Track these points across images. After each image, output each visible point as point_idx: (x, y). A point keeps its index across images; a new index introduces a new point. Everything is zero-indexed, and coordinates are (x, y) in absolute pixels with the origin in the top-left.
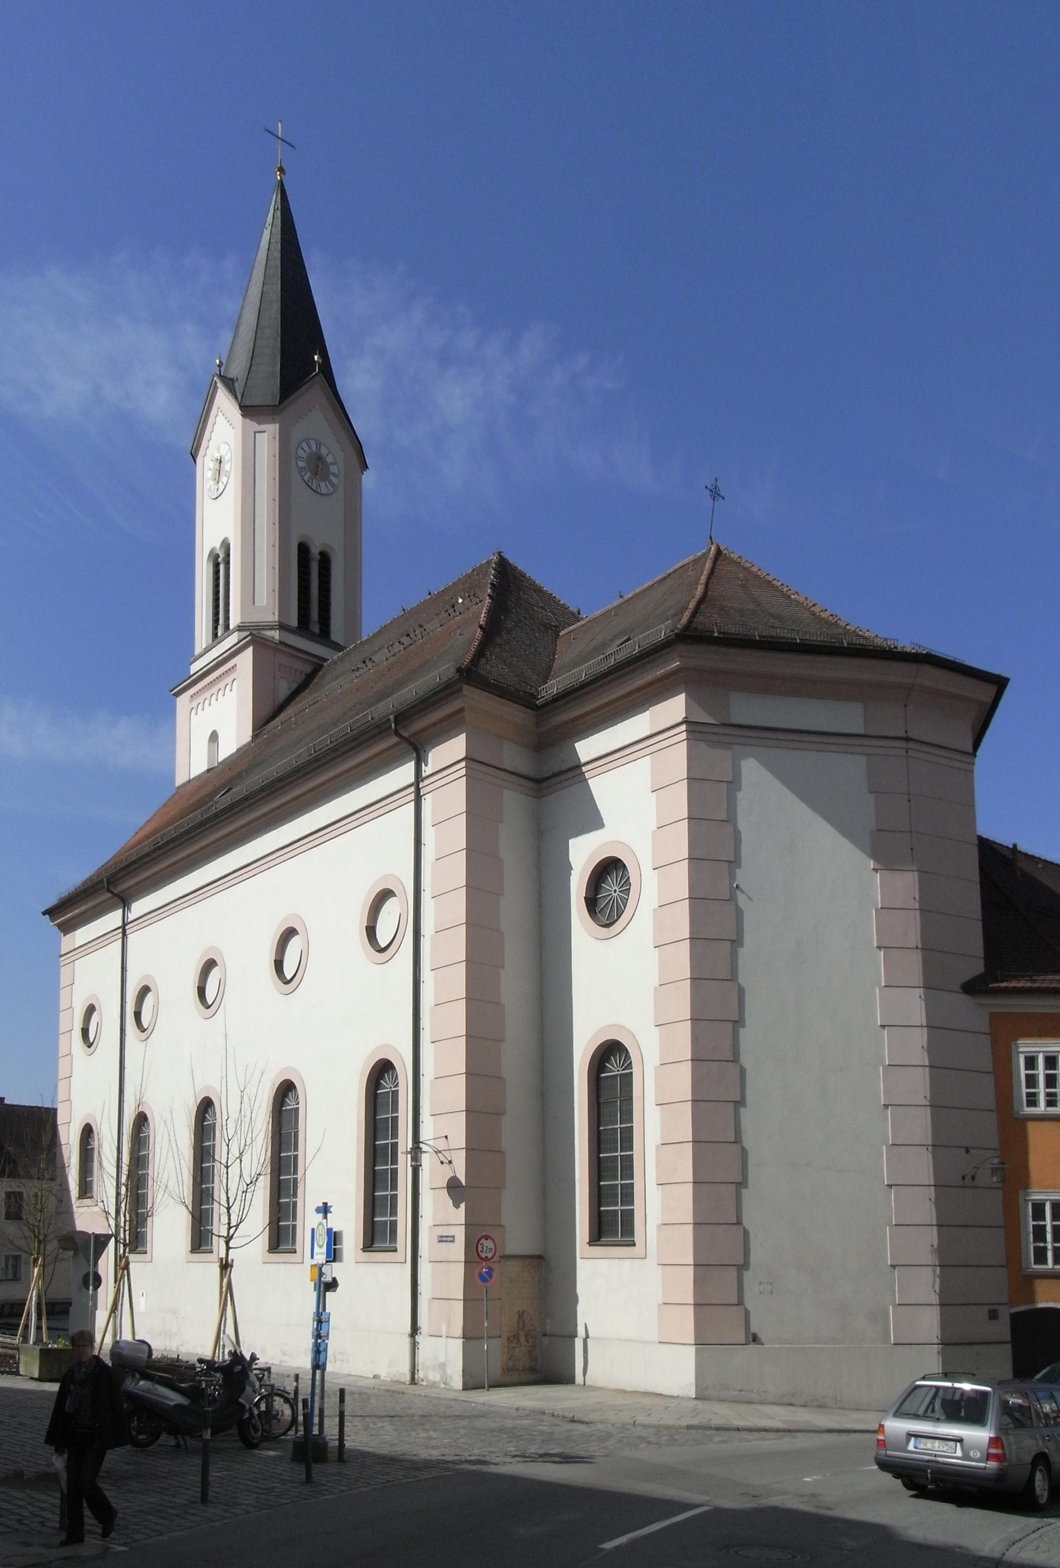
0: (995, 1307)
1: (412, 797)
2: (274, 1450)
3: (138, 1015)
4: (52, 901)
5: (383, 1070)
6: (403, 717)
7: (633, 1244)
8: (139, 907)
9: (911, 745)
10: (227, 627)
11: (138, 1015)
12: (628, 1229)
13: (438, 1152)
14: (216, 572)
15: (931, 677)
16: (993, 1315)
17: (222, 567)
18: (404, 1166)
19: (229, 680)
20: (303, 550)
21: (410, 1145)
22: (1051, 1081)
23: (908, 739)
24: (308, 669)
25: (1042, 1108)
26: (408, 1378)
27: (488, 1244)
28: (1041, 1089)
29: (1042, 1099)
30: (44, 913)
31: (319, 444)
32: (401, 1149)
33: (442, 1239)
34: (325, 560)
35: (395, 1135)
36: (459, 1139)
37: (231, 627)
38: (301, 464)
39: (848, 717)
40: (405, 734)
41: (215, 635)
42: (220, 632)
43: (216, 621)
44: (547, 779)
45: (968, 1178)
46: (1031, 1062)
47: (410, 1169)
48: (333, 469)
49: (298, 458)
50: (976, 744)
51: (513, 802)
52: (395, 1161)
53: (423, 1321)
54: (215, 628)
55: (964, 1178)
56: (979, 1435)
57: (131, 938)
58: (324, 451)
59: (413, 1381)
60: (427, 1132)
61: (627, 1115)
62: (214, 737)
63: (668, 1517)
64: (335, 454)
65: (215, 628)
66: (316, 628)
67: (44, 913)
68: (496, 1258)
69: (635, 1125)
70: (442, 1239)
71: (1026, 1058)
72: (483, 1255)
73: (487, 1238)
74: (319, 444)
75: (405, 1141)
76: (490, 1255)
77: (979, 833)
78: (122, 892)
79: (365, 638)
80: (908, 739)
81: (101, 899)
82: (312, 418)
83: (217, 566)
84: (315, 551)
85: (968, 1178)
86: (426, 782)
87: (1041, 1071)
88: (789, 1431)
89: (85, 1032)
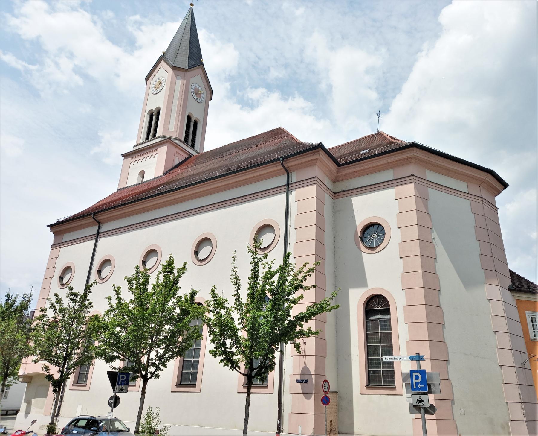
1: (285, 190)
3: (99, 272)
4: (54, 222)
10: (155, 135)
17: (154, 117)
20: (189, 118)
24: (187, 156)
30: (48, 226)
31: (199, 87)
34: (196, 124)
37: (157, 136)
39: (462, 186)
40: (286, 166)
41: (147, 138)
42: (150, 137)
44: (338, 192)
49: (191, 88)
51: (328, 199)
56: (145, 363)
58: (200, 89)
66: (190, 144)
67: (48, 226)
69: (393, 331)
72: (325, 390)
74: (199, 87)
78: (288, 167)
81: (88, 221)
82: (196, 79)
84: (193, 119)
86: (292, 185)
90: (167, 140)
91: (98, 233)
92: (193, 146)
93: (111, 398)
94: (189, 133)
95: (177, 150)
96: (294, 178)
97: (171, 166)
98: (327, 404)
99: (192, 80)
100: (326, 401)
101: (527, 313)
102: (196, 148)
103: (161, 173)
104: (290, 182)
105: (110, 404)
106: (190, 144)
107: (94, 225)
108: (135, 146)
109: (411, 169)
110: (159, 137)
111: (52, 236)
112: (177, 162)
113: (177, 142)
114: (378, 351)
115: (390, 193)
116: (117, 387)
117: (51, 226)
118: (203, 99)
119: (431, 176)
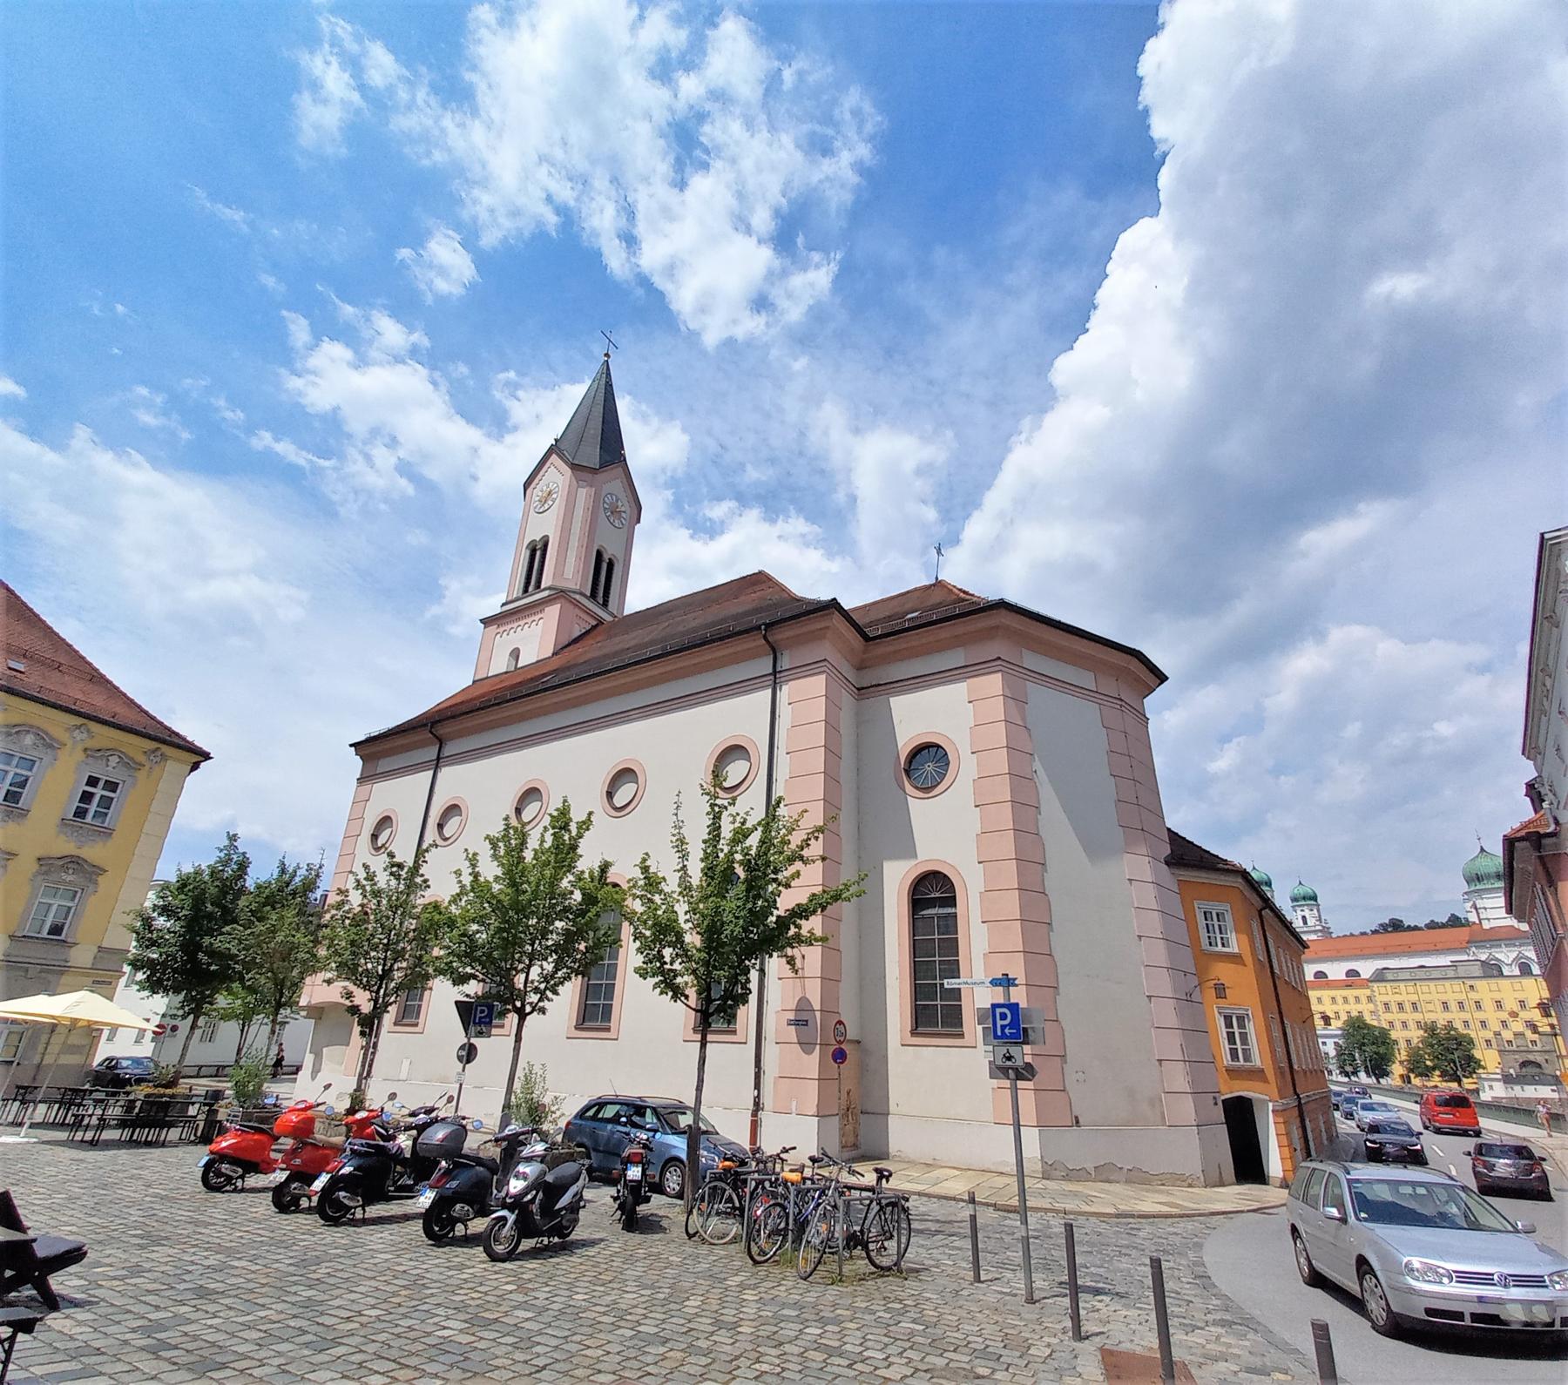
20: (599, 554)
34: (611, 565)
39: (1086, 679)
53: (767, 1100)
64: (624, 506)
84: (606, 557)
90: (560, 594)
91: (438, 758)
92: (605, 604)
93: (462, 1048)
95: (577, 611)
100: (839, 1056)
102: (610, 607)
105: (460, 1058)
111: (358, 762)
113: (577, 597)
115: (957, 691)
116: (472, 1029)
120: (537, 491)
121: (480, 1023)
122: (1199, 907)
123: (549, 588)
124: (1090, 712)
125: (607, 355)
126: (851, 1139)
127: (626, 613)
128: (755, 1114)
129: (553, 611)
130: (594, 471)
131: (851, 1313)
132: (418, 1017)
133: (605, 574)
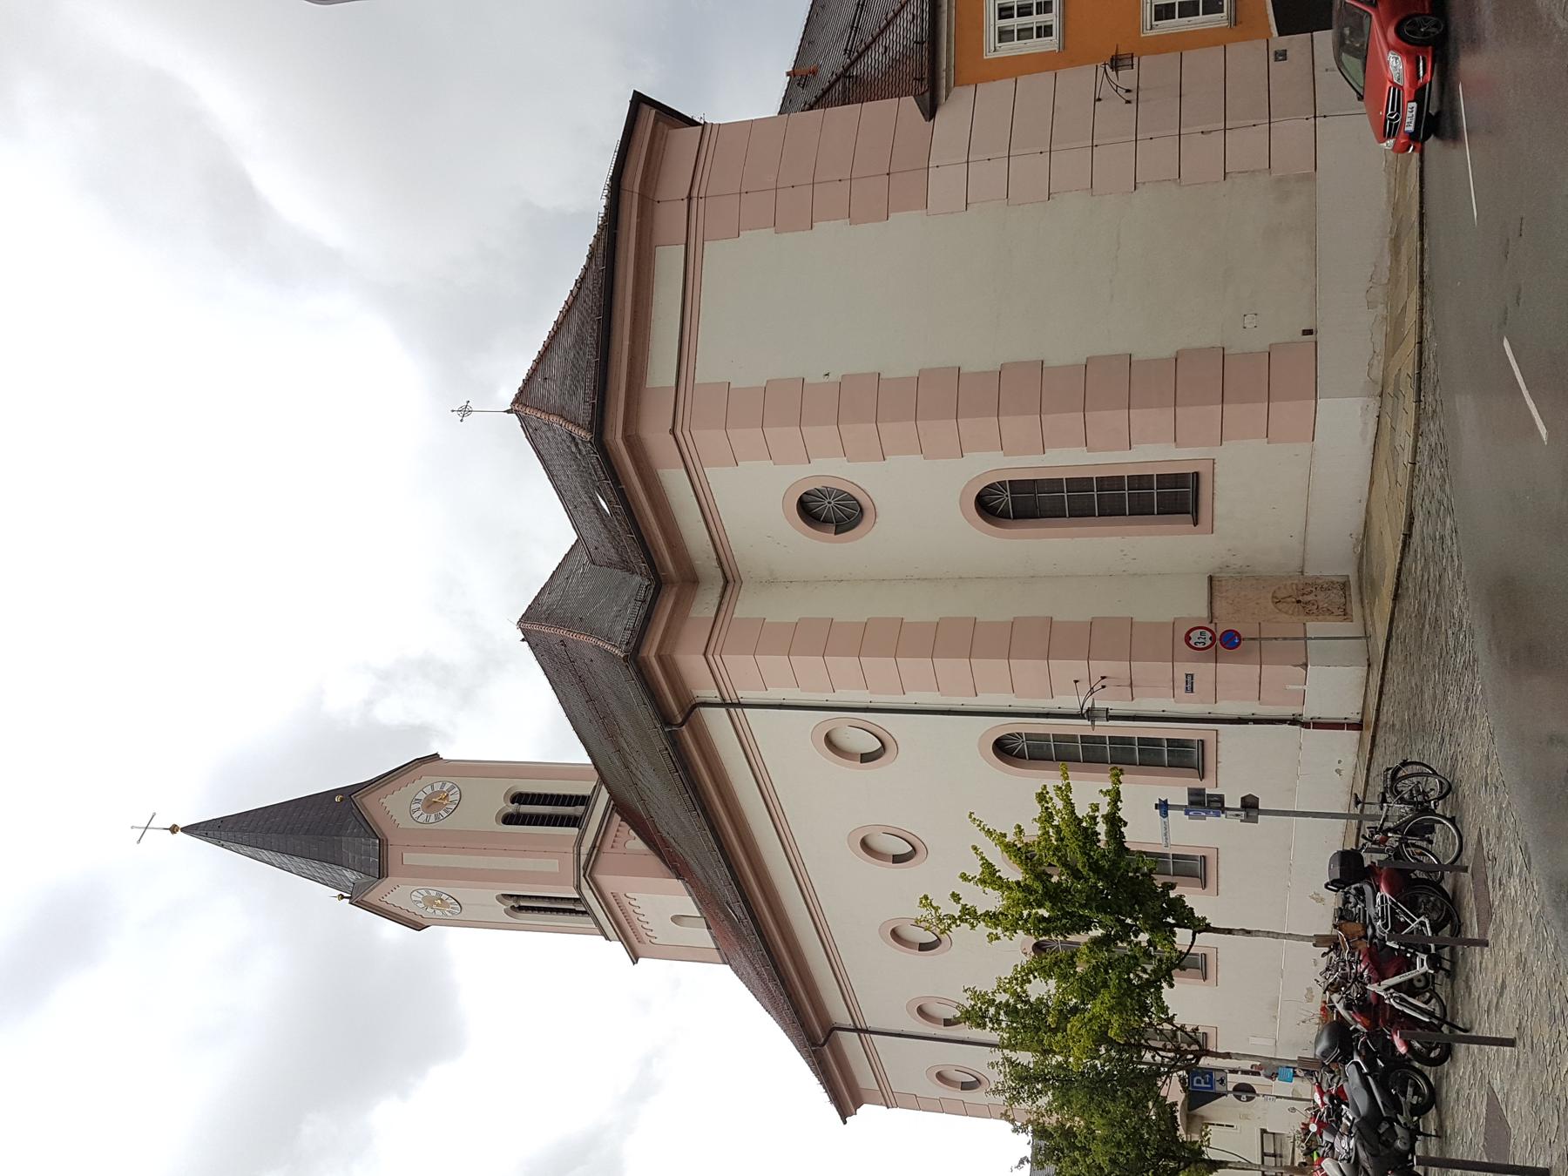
0: (1272, 57)
2: (608, 503)
5: (1004, 749)
6: (665, 719)
7: (1197, 474)
8: (840, 1015)
9: (695, 194)
11: (947, 1023)
12: (1178, 480)
13: (1092, 691)
14: (527, 909)
15: (634, 180)
16: (1282, 55)
18: (1105, 729)
19: (625, 901)
20: (509, 819)
21: (1086, 722)
22: (1025, 11)
23: (690, 198)
24: (617, 818)
25: (1052, 18)
26: (1355, 734)
27: (1195, 635)
28: (1034, 20)
29: (1044, 18)
32: (1089, 732)
33: (1190, 689)
34: (519, 798)
35: (1073, 738)
36: (1078, 668)
38: (432, 819)
39: (669, 261)
43: (571, 911)
45: (1128, 96)
46: (1004, 35)
47: (1111, 723)
48: (437, 787)
49: (427, 821)
50: (692, 123)
52: (1101, 739)
53: (1287, 711)
54: (577, 912)
55: (1128, 102)
57: (871, 1025)
58: (422, 796)
59: (1358, 726)
60: (1071, 703)
61: (1055, 484)
62: (676, 919)
63: (1533, 419)
64: (423, 786)
65: (577, 912)
66: (579, 810)
68: (1212, 627)
70: (1190, 689)
71: (1001, 18)
72: (1209, 642)
73: (1188, 638)
75: (1081, 728)
76: (1208, 635)
77: (771, 108)
79: (589, 761)
80: (690, 198)
83: (521, 908)
84: (512, 808)
85: (1128, 96)
87: (1015, 22)
88: (1422, 282)
89: (966, 1086)
90: (587, 869)
91: (856, 1030)
92: (582, 800)
93: (1239, 1098)
94: (550, 816)
95: (607, 847)
96: (711, 694)
97: (654, 861)
98: (1237, 634)
99: (404, 822)
100: (1231, 640)
101: (992, 55)
102: (588, 792)
103: (678, 884)
104: (719, 700)
105: (1249, 1099)
106: (582, 808)
107: (837, 1039)
108: (607, 938)
109: (656, 437)
110: (580, 893)
111: (865, 1109)
112: (637, 844)
113: (585, 850)
114: (1160, 753)
115: (719, 479)
116: (1219, 1088)
117: (844, 1115)
118: (448, 785)
119: (661, 372)
120: (418, 910)
121: (1211, 1081)
122: (994, 50)
123: (578, 888)
124: (717, 256)
125: (174, 829)
126: (1336, 596)
127: (581, 757)
128: (1306, 725)
129: (608, 881)
130: (383, 844)
131: (1496, 825)
132: (1193, 858)
133: (535, 806)
